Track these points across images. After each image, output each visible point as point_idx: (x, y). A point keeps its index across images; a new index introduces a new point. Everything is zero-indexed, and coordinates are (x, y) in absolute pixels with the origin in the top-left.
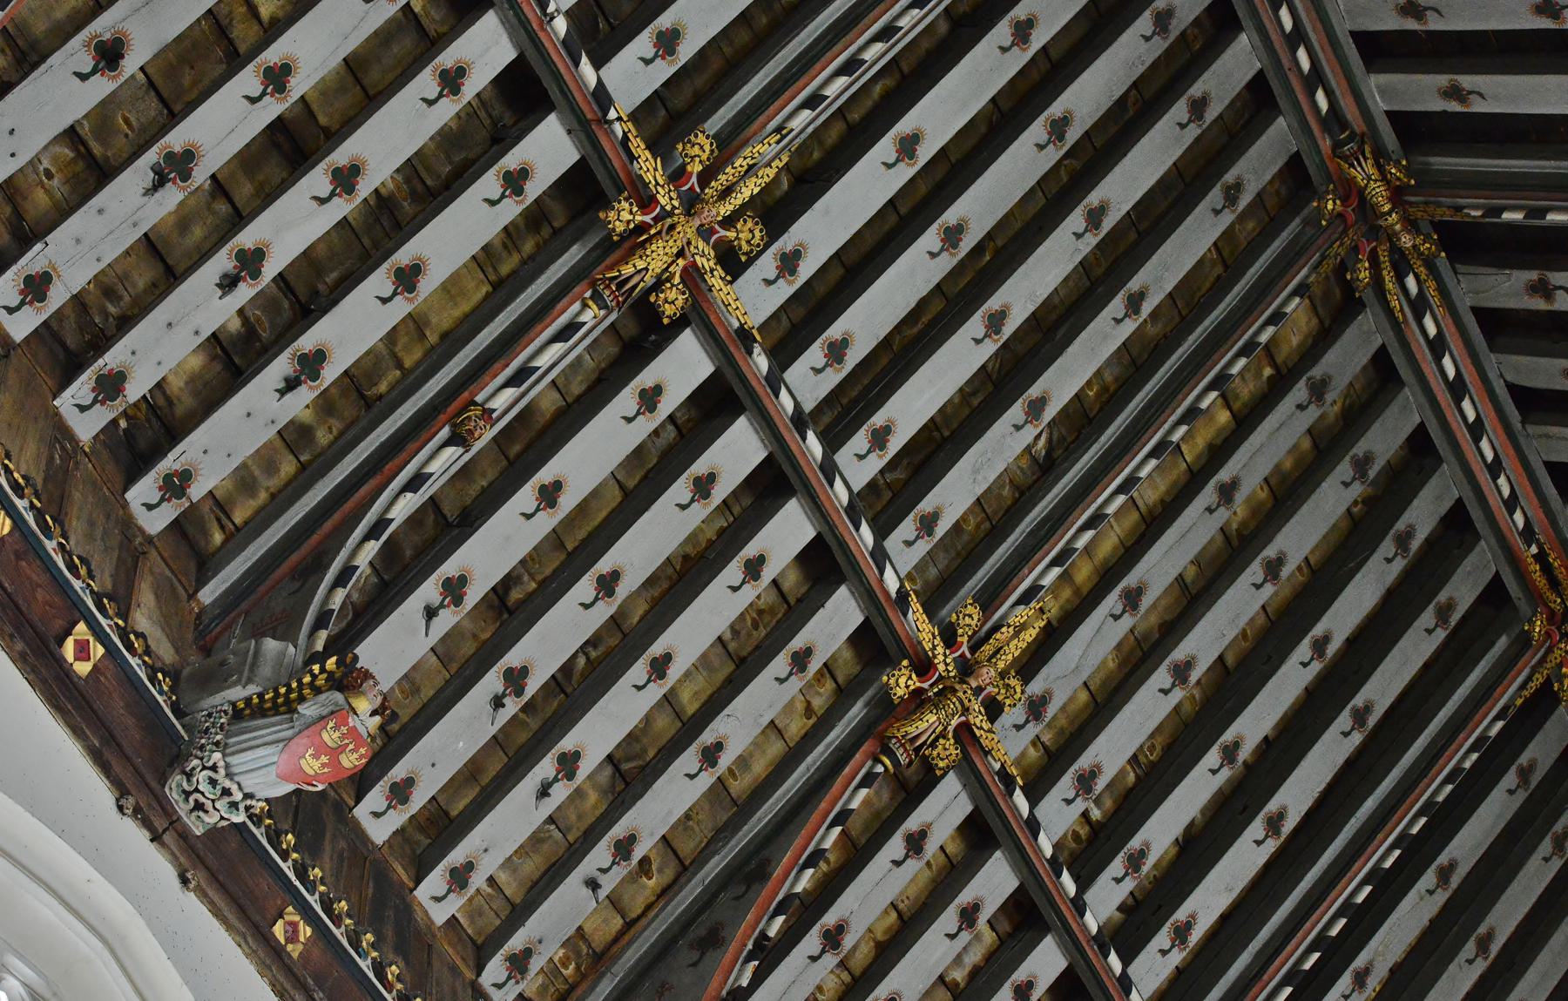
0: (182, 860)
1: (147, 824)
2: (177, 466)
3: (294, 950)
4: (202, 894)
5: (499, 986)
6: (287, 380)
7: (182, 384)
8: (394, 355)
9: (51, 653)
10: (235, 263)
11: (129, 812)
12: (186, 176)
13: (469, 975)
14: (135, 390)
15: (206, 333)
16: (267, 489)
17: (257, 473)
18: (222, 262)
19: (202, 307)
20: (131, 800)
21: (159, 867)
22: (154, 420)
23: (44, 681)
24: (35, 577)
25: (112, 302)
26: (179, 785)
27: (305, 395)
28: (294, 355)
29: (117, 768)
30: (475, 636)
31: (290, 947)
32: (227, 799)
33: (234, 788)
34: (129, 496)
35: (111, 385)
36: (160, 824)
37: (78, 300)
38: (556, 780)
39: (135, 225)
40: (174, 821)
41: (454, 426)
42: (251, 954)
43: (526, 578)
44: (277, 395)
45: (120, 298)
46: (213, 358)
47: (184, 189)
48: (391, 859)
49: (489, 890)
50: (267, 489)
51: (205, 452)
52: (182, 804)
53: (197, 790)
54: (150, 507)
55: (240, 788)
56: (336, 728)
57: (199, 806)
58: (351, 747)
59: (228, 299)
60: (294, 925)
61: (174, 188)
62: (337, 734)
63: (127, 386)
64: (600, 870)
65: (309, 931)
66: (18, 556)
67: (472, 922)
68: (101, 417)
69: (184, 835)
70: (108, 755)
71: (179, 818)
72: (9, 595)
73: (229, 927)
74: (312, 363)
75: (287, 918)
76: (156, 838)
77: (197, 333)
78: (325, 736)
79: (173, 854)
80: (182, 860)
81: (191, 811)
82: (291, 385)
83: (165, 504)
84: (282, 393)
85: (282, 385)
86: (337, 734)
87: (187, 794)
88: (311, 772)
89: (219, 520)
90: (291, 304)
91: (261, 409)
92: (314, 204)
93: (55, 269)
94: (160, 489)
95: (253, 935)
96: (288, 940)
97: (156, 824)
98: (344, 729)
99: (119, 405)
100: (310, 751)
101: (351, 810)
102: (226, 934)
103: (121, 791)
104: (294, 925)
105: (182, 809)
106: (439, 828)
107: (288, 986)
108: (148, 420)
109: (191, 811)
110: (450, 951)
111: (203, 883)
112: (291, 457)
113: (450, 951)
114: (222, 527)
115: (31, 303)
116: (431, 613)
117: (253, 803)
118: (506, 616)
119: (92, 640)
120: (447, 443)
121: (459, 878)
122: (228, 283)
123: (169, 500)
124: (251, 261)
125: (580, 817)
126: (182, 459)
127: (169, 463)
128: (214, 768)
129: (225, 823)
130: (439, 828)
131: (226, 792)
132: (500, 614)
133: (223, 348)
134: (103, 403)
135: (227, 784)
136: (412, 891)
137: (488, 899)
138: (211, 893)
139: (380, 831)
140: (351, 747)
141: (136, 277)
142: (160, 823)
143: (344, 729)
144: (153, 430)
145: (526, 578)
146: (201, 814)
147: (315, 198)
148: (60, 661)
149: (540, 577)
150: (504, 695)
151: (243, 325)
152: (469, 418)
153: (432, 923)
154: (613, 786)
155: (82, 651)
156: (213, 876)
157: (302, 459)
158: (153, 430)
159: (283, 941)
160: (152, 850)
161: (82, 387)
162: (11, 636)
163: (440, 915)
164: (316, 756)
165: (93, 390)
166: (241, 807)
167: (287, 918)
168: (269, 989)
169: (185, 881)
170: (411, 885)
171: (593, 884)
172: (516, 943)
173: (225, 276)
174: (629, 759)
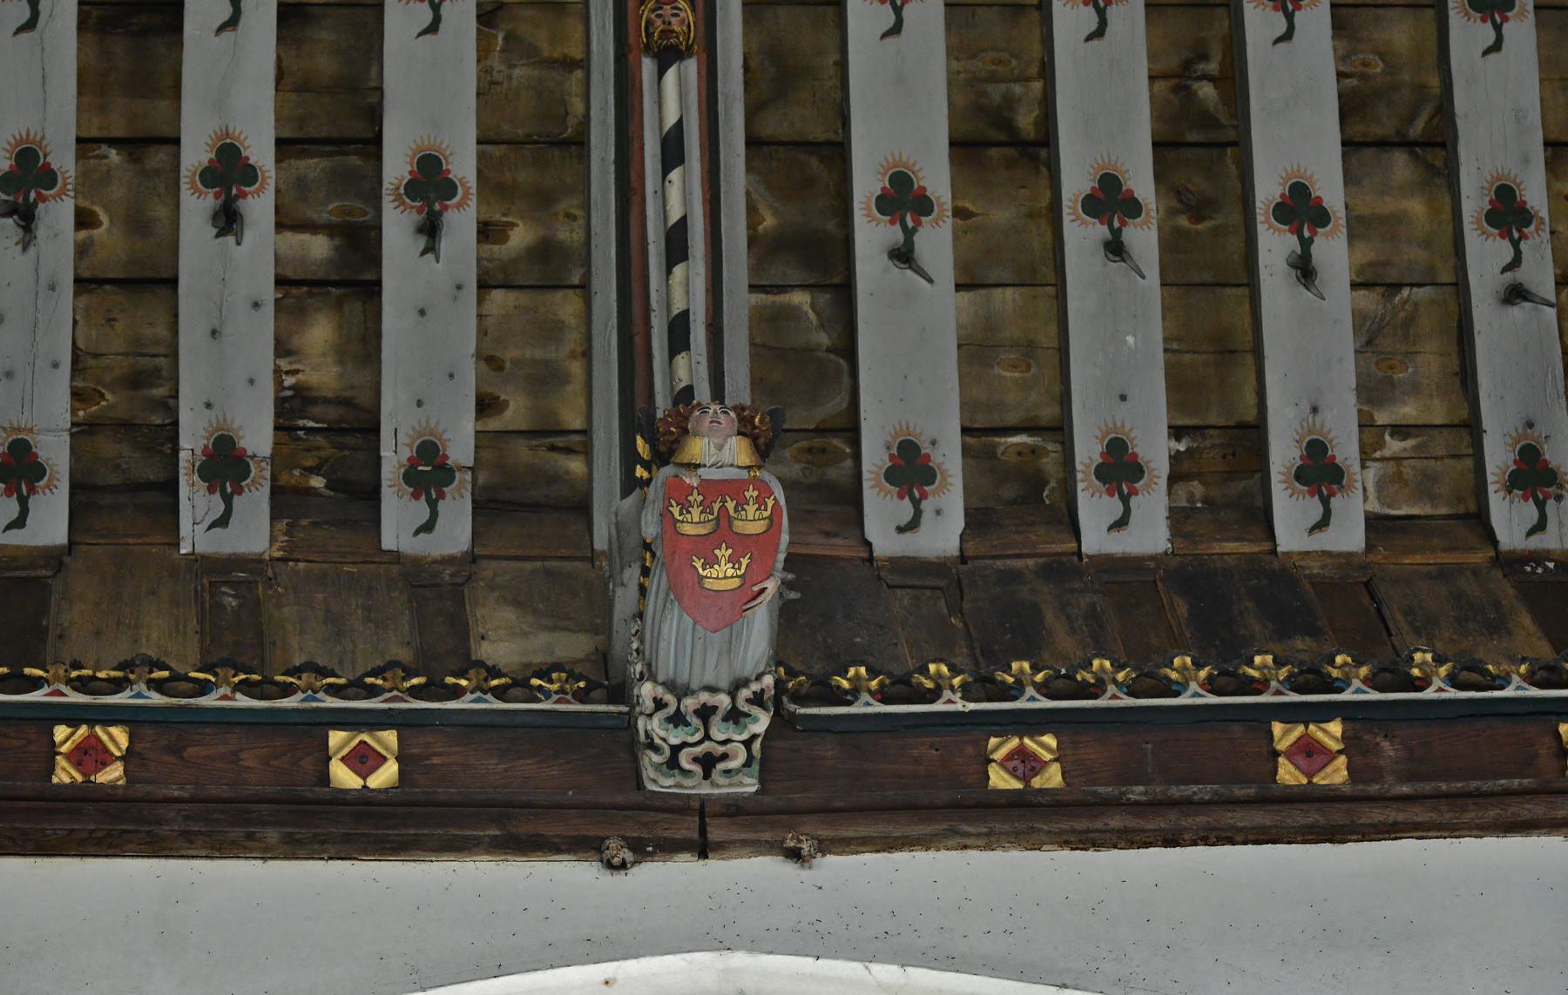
0: (767, 836)
1: (669, 848)
2: (406, 453)
3: (1052, 778)
4: (825, 847)
5: (1540, 526)
6: (420, 230)
7: (335, 369)
8: (551, 63)
9: (331, 802)
10: (211, 192)
11: (628, 855)
12: (48, 178)
13: (1480, 557)
14: (258, 438)
15: (269, 293)
16: (572, 355)
17: (539, 354)
18: (196, 207)
19: (230, 277)
20: (613, 843)
21: (755, 873)
22: (350, 440)
23: (347, 839)
24: (222, 749)
25: (152, 386)
26: (657, 767)
27: (461, 223)
28: (398, 198)
29: (552, 830)
30: (1031, 215)
31: (1037, 782)
32: (716, 720)
33: (705, 697)
34: (388, 542)
35: (225, 466)
36: (687, 829)
37: (82, 431)
38: (1306, 244)
39: (52, 288)
40: (702, 810)
41: (647, 49)
42: (990, 842)
43: (1017, 89)
44: (430, 256)
45: (157, 370)
46: (339, 305)
47: (63, 192)
48: (1202, 549)
49: (1410, 443)
50: (572, 355)
51: (419, 404)
52: (688, 782)
53: (675, 750)
54: (428, 527)
55: (713, 690)
56: (685, 507)
57: (708, 763)
58: (730, 505)
59: (248, 235)
60: (1021, 754)
61: (51, 204)
62: (696, 513)
63: (242, 444)
64: (1507, 268)
65: (1049, 740)
66: (176, 750)
67: (1433, 498)
68: (255, 504)
69: (734, 809)
70: (523, 829)
71: (704, 800)
72: (192, 800)
73: (925, 843)
74: (430, 181)
75: (1282, 745)
76: (703, 850)
77: (256, 305)
78: (688, 529)
79: (744, 843)
80: (767, 836)
81: (707, 776)
82: (430, 230)
83: (441, 505)
84: (431, 249)
85: (422, 242)
86: (696, 513)
87: (673, 763)
88: (736, 583)
89: (553, 448)
90: (356, 153)
91: (428, 288)
92: (228, 35)
93: (19, 430)
94: (416, 496)
95: (965, 820)
96: (1026, 779)
97: (679, 835)
98: (696, 497)
99: (261, 475)
100: (698, 564)
101: (1079, 553)
102: (932, 854)
103: (585, 846)
104: (1021, 754)
105: (698, 787)
106: (1225, 453)
107: (1081, 825)
108: (342, 447)
109: (707, 776)
110: (1418, 559)
111: (825, 833)
112: (559, 294)
113: (1418, 559)
114: (568, 451)
115: (32, 490)
116: (903, 255)
117: (755, 687)
118: (1043, 153)
119: (365, 737)
120: (661, 73)
121: (1320, 472)
122: (228, 220)
123: (441, 495)
124: (229, 170)
125: (1427, 244)
126: (402, 438)
127: (393, 458)
128: (659, 704)
129: (757, 746)
130: (1225, 453)
131: (705, 713)
132: (1035, 159)
133: (335, 284)
134: (239, 490)
135: (690, 704)
136: (1274, 552)
137: (1420, 453)
138: (850, 833)
139: (1150, 534)
140: (730, 505)
141: (148, 331)
142: (699, 830)
143: (696, 497)
144: (331, 446)
145: (1017, 89)
146: (721, 766)
147: (222, 28)
148: (344, 798)
149: (1034, 70)
150: (1116, 233)
151: (331, 236)
152: (649, 23)
153: (1350, 554)
154: (1430, 167)
155: (364, 760)
156: (826, 811)
157: (576, 280)
158: (331, 446)
159: (1018, 785)
160: (716, 868)
161: (195, 503)
162: (250, 836)
163: (1348, 536)
164: (711, 561)
165: (211, 490)
166: (744, 707)
167: (1282, 745)
168: (1066, 854)
169: (795, 855)
170: (1266, 546)
171: (1516, 294)
172: (1498, 457)
173: (215, 217)
174: (1411, 120)
